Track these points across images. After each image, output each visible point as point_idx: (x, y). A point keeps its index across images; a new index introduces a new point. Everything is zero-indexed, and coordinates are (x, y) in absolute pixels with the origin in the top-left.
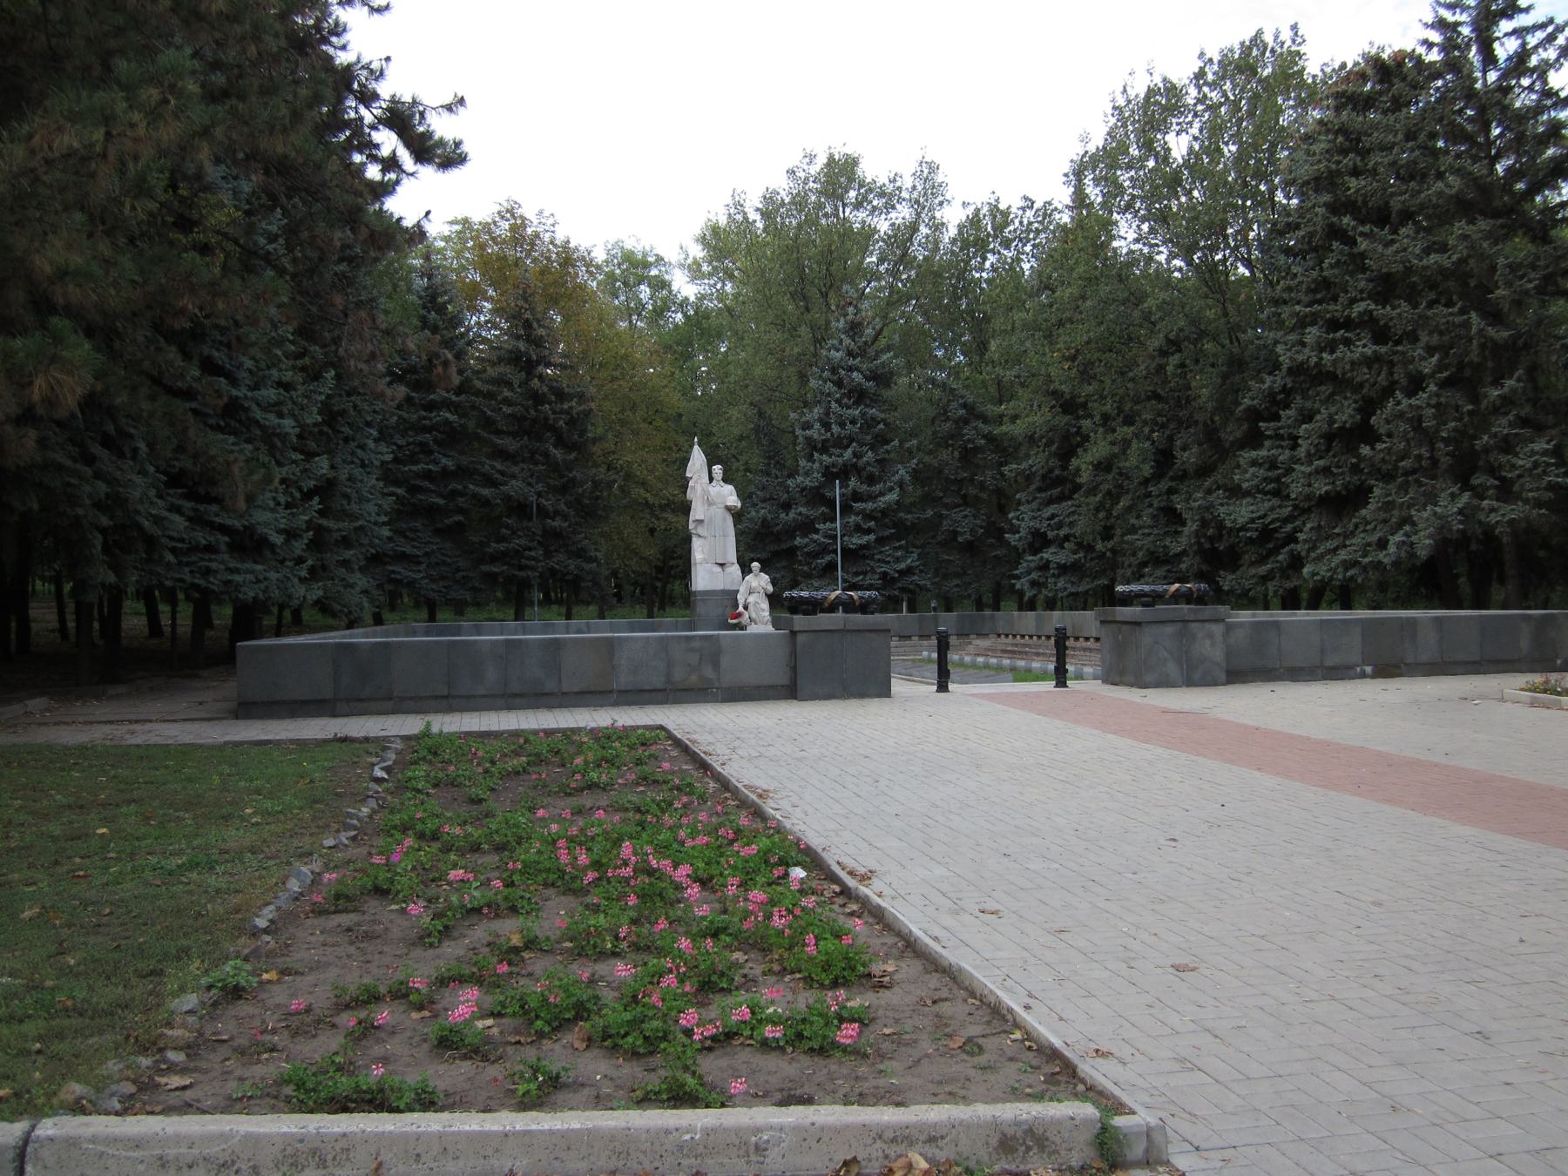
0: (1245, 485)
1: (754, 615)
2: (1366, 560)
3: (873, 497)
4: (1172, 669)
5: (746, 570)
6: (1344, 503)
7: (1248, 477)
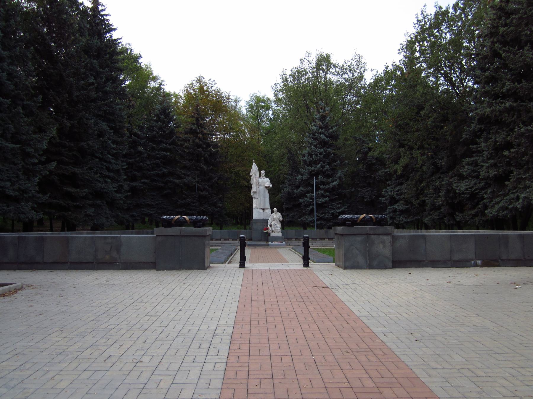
0: (464, 174)
1: (273, 229)
2: (510, 206)
3: (328, 183)
4: (360, 259)
5: (272, 212)
6: (500, 180)
7: (465, 170)
